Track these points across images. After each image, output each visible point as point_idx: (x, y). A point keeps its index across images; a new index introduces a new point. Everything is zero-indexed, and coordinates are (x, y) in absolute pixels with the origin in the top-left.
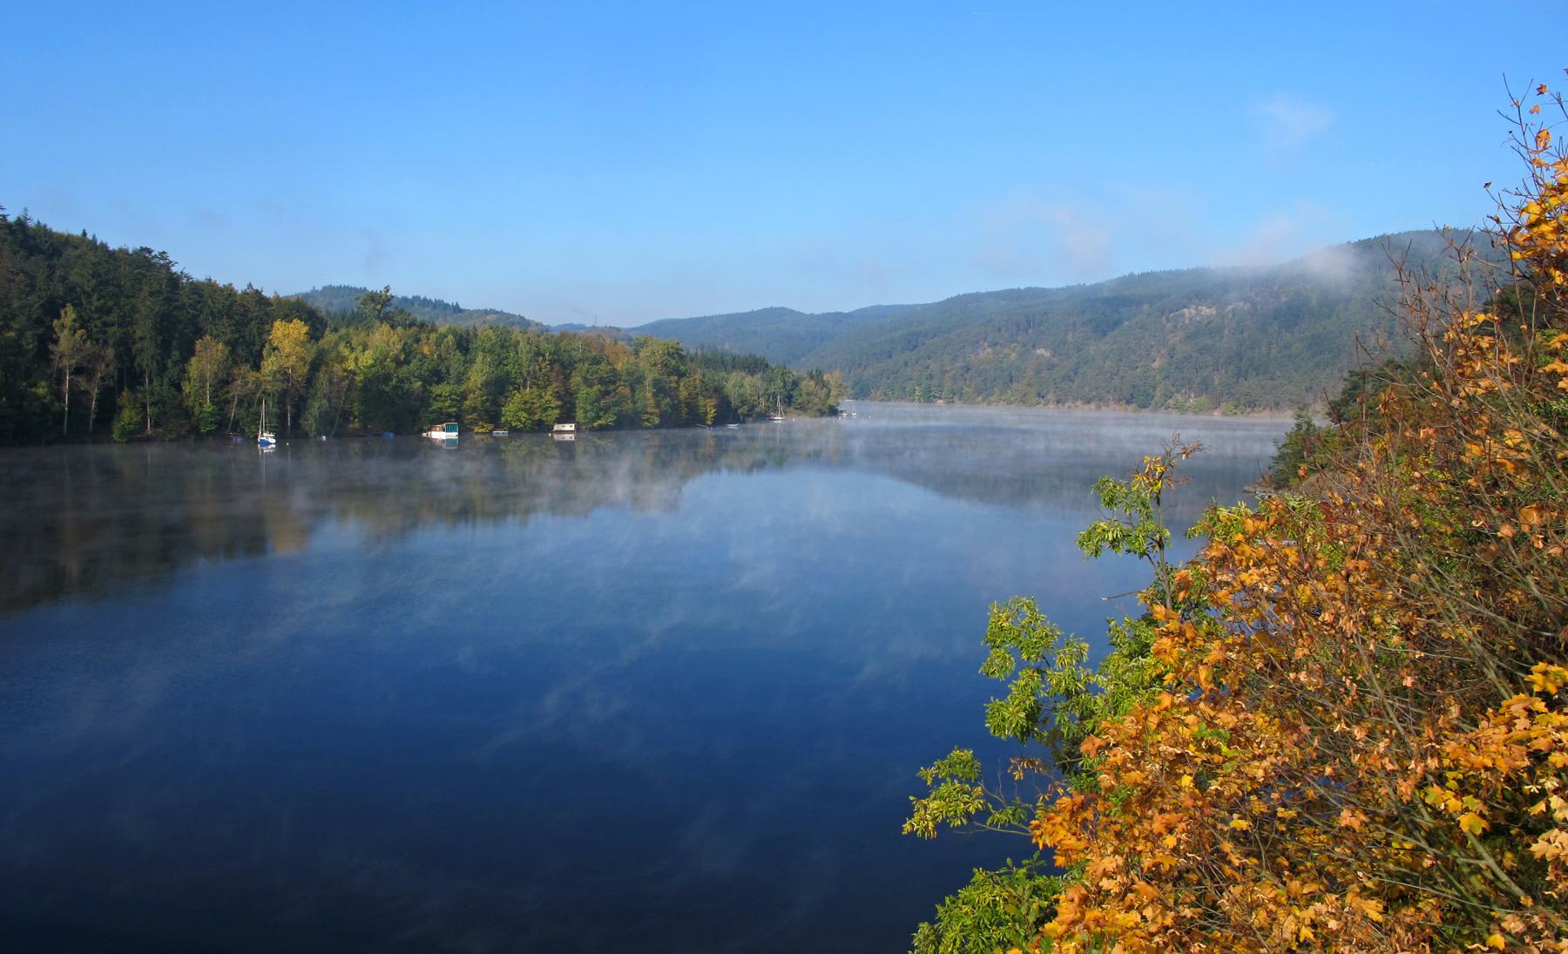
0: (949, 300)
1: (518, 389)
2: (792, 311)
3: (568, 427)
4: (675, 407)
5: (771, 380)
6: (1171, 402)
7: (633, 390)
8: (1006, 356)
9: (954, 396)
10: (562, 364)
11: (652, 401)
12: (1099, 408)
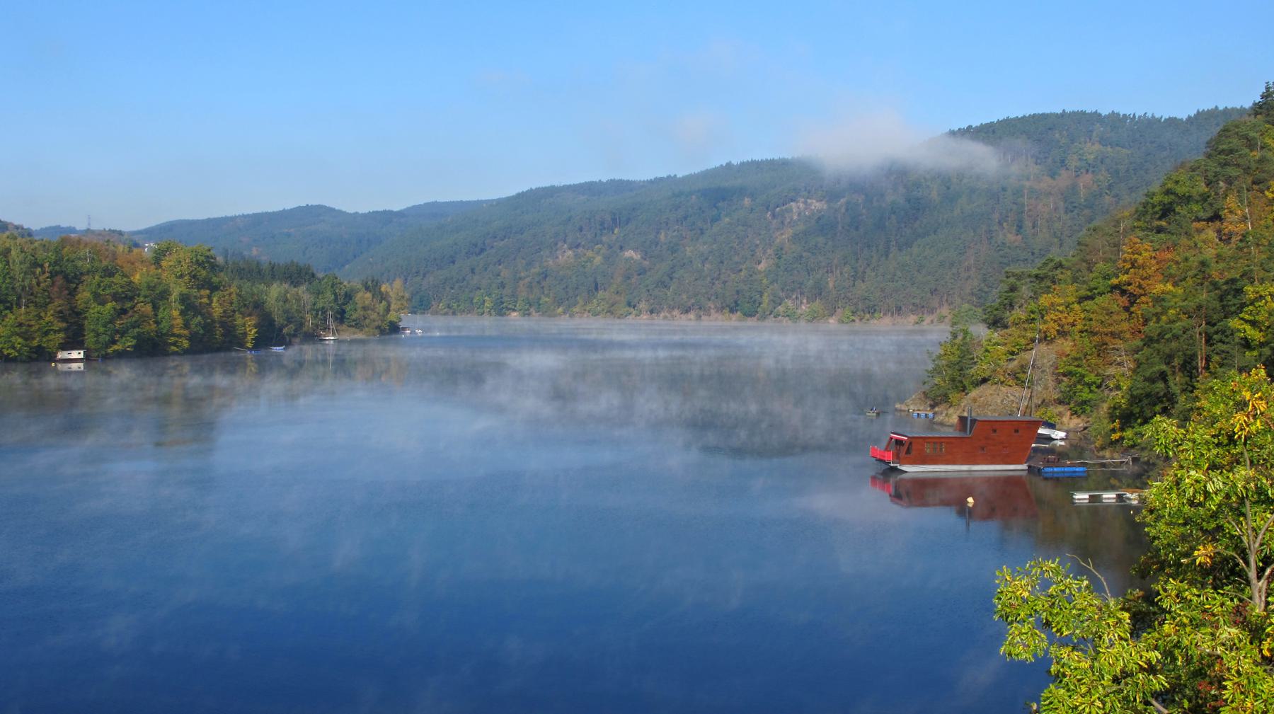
0: (520, 196)
1: (10, 308)
2: (332, 210)
3: (76, 354)
4: (208, 328)
5: (319, 293)
6: (781, 309)
7: (155, 308)
8: (590, 260)
9: (531, 306)
10: (66, 278)
11: (179, 321)
12: (699, 317)
